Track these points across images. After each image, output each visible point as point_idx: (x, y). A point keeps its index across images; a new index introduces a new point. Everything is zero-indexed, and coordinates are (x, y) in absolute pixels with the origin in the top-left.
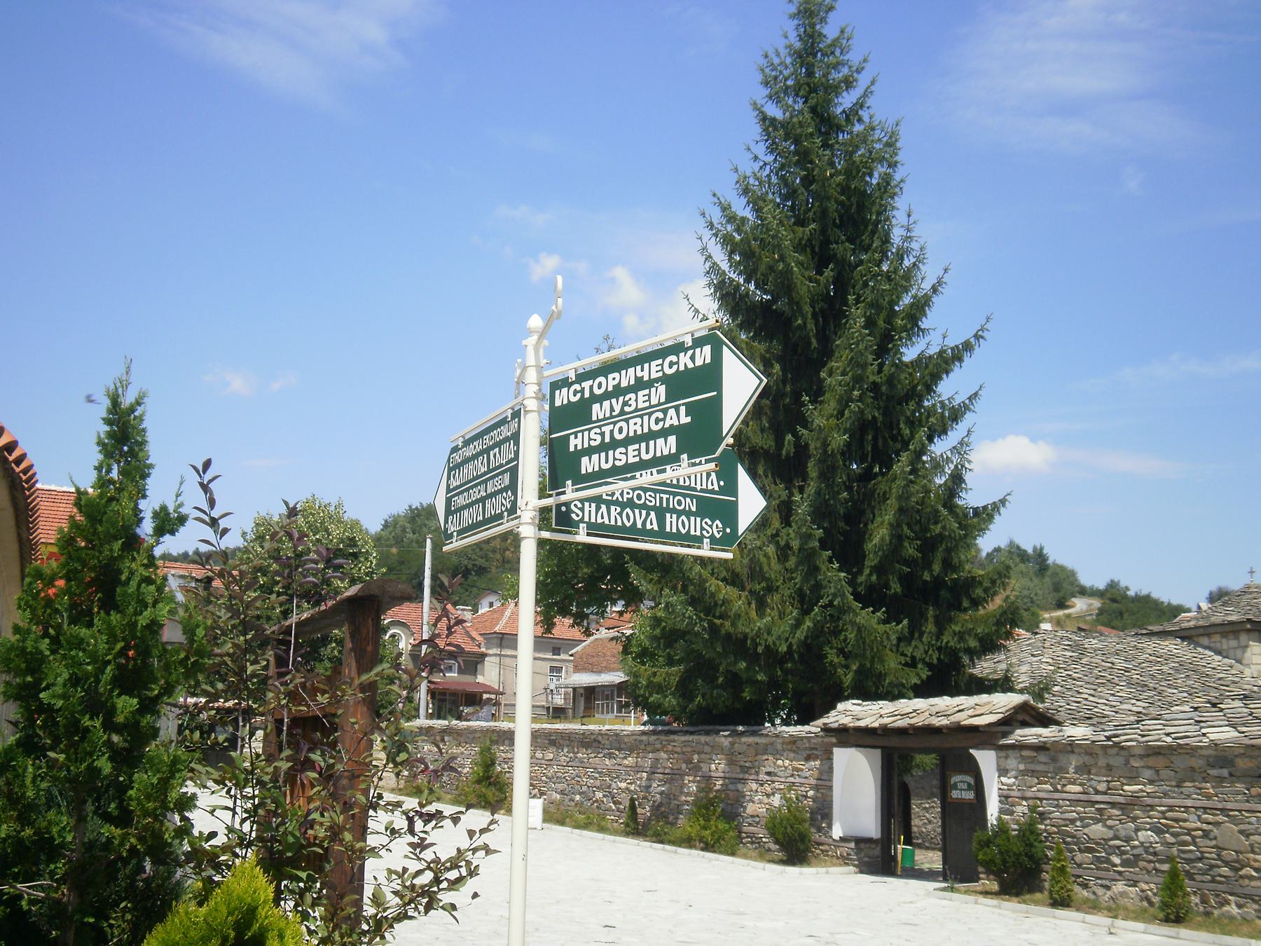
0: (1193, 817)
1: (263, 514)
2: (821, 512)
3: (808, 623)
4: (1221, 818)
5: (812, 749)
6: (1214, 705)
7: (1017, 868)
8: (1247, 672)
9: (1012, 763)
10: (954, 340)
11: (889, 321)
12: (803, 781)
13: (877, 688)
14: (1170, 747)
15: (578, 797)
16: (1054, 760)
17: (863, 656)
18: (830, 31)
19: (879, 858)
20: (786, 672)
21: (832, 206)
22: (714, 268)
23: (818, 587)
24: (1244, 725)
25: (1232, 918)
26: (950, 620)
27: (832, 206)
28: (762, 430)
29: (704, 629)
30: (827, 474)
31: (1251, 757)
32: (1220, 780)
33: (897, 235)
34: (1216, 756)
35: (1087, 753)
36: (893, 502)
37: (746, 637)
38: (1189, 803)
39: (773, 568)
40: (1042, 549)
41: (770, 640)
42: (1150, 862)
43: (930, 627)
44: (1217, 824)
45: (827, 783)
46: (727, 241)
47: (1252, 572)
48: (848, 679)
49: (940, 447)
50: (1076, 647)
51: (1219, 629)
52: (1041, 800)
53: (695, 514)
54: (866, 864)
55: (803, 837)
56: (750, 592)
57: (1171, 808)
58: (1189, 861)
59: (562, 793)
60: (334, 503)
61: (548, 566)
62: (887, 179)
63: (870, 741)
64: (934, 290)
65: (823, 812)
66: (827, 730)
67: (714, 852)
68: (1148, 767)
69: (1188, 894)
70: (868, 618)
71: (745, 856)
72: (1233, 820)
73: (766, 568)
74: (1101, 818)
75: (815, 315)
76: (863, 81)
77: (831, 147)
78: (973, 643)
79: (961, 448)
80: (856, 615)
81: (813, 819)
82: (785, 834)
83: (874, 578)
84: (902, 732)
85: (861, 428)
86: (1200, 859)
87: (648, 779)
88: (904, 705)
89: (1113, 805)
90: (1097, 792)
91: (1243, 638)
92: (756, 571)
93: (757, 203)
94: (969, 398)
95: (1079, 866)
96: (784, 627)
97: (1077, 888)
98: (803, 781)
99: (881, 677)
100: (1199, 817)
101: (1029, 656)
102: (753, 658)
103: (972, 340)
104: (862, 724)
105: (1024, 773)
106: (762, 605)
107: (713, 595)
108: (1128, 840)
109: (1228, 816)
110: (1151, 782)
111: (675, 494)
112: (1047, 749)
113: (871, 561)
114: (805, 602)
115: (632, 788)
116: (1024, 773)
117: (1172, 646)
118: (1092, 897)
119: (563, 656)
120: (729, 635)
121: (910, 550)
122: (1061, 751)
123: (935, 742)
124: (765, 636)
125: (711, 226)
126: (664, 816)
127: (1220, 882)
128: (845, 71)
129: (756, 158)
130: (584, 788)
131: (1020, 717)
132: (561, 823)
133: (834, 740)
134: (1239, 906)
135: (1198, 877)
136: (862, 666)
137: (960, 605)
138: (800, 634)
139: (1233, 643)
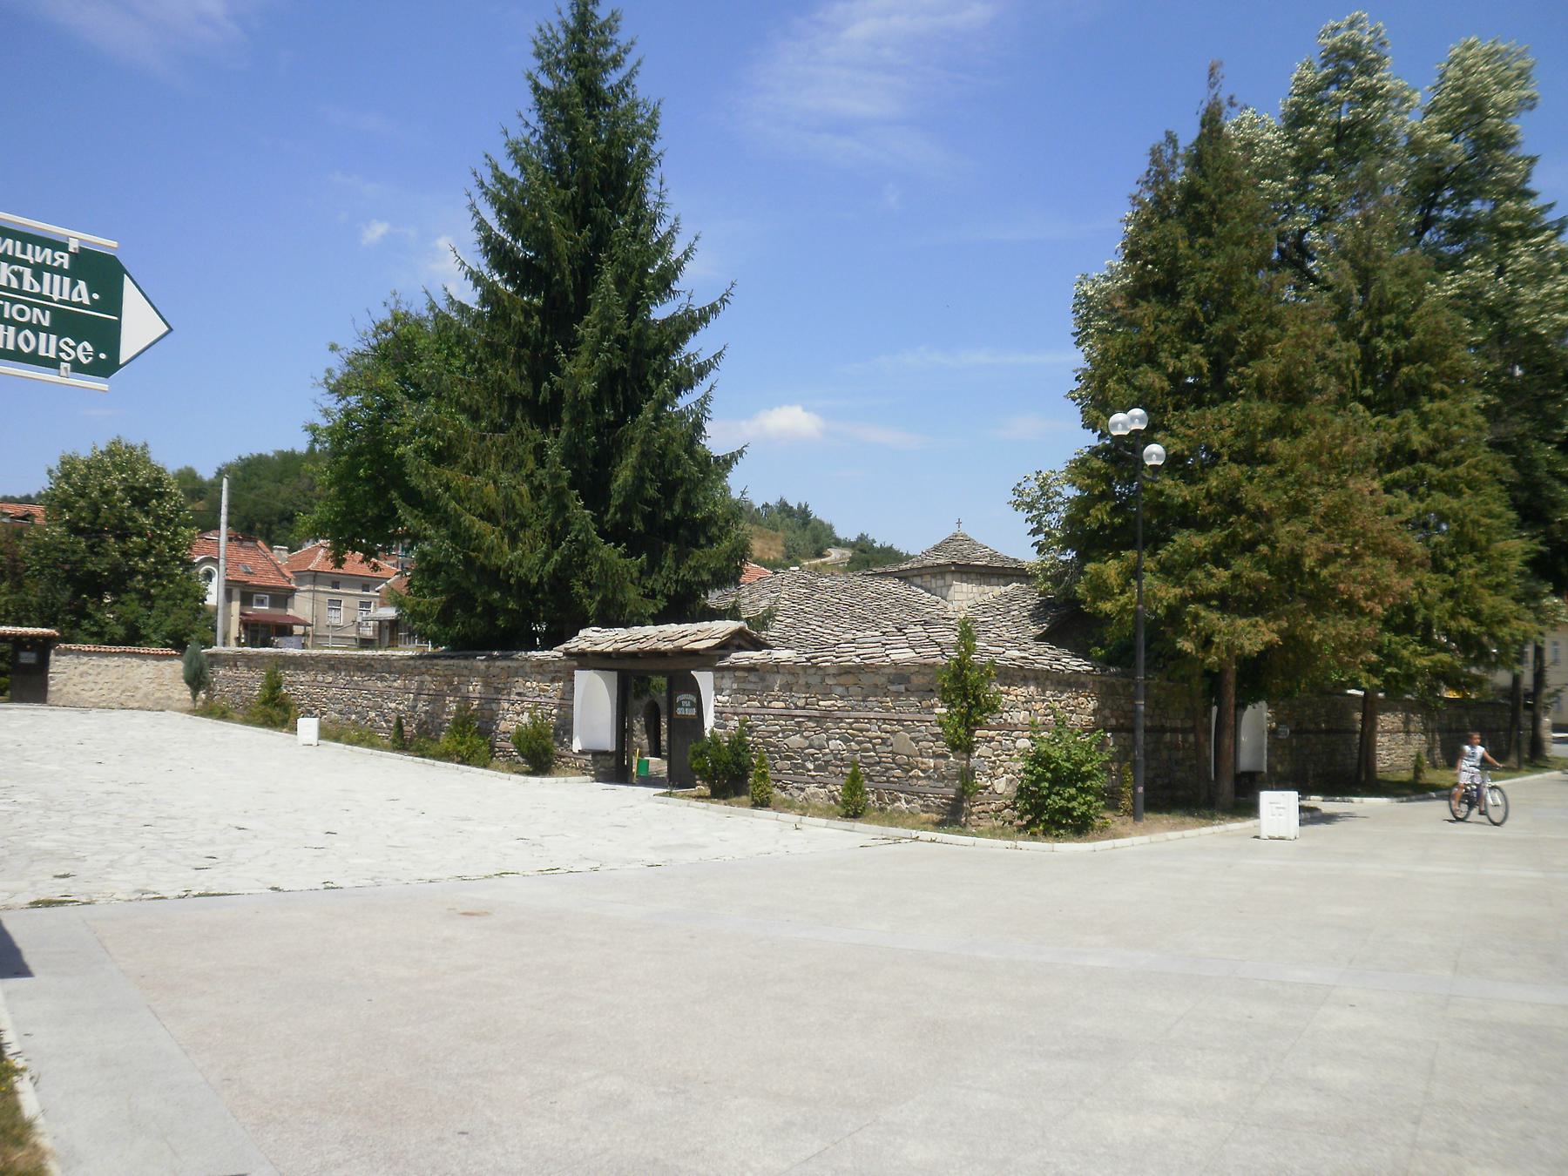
1: (69, 452)
2: (572, 455)
3: (556, 557)
4: (897, 728)
7: (729, 775)
8: (950, 607)
9: (727, 683)
10: (699, 303)
11: (640, 281)
14: (858, 667)
16: (763, 679)
17: (605, 587)
18: (602, 13)
19: (614, 768)
20: (538, 602)
21: (594, 172)
22: (482, 225)
23: (567, 523)
25: (902, 812)
27: (594, 172)
28: (522, 378)
30: (576, 421)
32: (899, 694)
33: (651, 198)
36: (636, 449)
37: (499, 568)
38: (872, 715)
39: (525, 506)
43: (669, 562)
44: (893, 733)
46: (494, 199)
48: (592, 608)
49: (685, 401)
50: (811, 586)
53: (47, 330)
55: (547, 751)
56: (505, 528)
57: (857, 720)
58: (869, 765)
59: (340, 712)
60: (140, 444)
62: (645, 151)
63: (607, 664)
64: (686, 254)
65: (565, 728)
66: (567, 653)
70: (608, 552)
71: (496, 769)
72: (907, 729)
73: (518, 505)
75: (573, 273)
76: (629, 61)
77: (595, 117)
78: (706, 577)
79: (704, 402)
81: (556, 735)
82: (530, 748)
84: (633, 655)
85: (610, 380)
88: (637, 632)
89: (810, 718)
90: (797, 707)
91: (949, 578)
92: (511, 511)
93: (523, 162)
95: (780, 771)
96: (534, 559)
97: (776, 791)
99: (623, 606)
101: (759, 589)
102: (505, 587)
104: (598, 648)
105: (737, 691)
106: (514, 540)
107: (467, 529)
108: (821, 748)
110: (842, 698)
111: (13, 302)
113: (616, 501)
114: (555, 536)
116: (737, 691)
117: (890, 585)
119: (371, 593)
120: (483, 568)
121: (651, 491)
123: (661, 664)
125: (482, 185)
126: (427, 733)
128: (613, 50)
129: (527, 125)
131: (736, 642)
132: (337, 739)
134: (908, 802)
136: (605, 596)
138: (549, 567)
139: (940, 583)
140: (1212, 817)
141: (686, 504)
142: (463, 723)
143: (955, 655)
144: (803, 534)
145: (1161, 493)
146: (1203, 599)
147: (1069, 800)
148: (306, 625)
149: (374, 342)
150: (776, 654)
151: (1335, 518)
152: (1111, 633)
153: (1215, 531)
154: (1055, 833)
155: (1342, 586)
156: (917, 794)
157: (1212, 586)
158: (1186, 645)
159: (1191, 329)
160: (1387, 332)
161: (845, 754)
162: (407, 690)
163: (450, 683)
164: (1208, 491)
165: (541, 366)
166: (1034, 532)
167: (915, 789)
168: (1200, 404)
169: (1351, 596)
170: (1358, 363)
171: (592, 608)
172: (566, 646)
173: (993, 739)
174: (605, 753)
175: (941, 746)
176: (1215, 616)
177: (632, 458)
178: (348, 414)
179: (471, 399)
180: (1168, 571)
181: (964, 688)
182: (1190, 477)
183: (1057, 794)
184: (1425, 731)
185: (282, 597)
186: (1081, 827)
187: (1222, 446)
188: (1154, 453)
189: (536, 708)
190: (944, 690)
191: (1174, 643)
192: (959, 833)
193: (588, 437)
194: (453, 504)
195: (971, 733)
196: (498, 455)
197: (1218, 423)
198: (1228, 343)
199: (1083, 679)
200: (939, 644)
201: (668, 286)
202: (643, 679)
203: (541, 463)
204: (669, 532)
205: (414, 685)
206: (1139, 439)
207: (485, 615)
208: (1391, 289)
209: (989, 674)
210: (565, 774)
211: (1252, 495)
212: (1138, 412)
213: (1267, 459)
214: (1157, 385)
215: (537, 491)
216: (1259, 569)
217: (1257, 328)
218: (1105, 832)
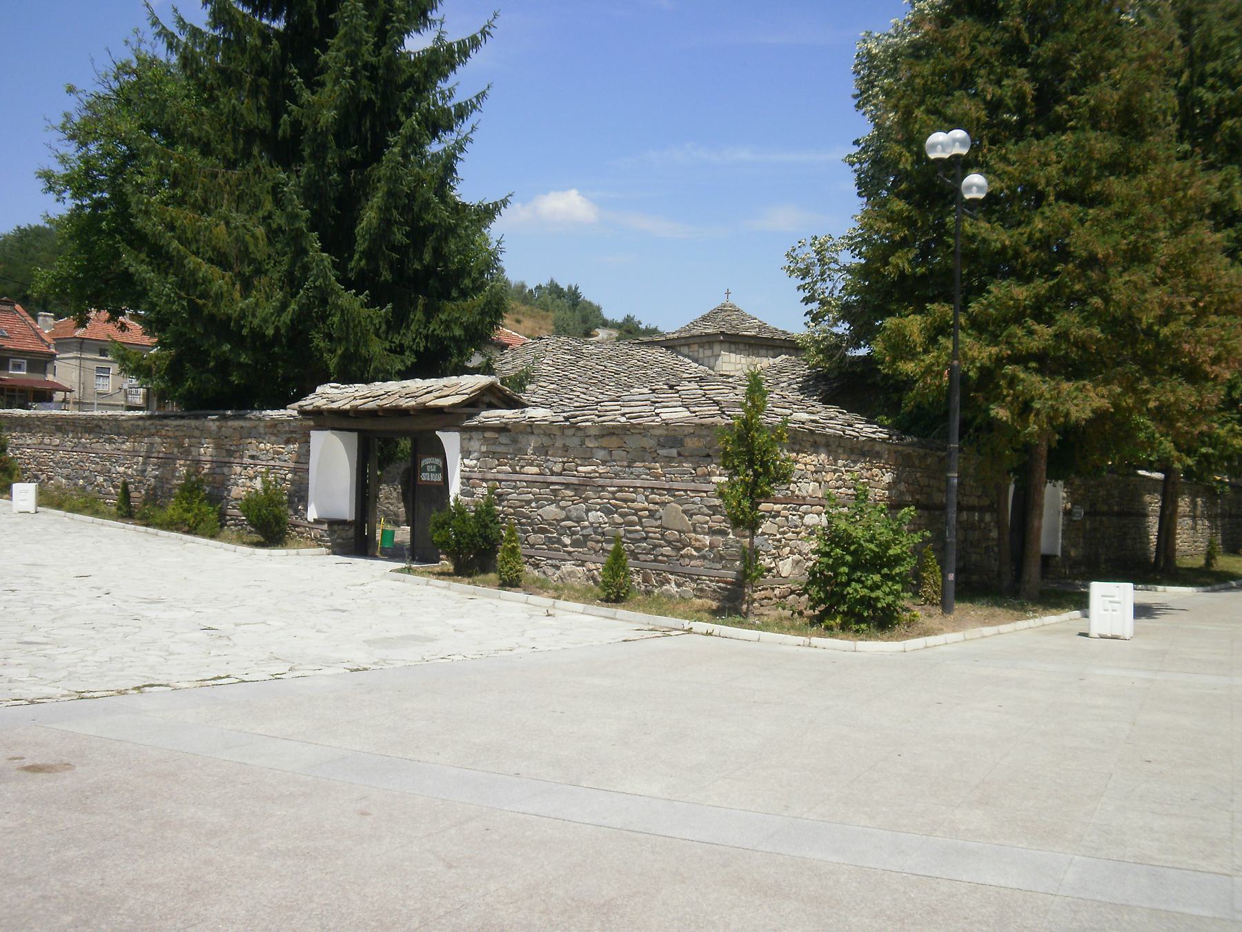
0: (641, 498)
2: (312, 193)
3: (294, 306)
4: (667, 498)
5: (292, 432)
6: (671, 387)
7: (473, 549)
9: (476, 445)
12: (282, 464)
13: (363, 374)
15: (81, 482)
16: (515, 441)
19: (354, 539)
23: (306, 269)
24: (696, 405)
25: (671, 597)
26: (438, 310)
28: (259, 110)
29: (183, 308)
31: (700, 436)
32: (670, 459)
34: (667, 436)
35: (545, 434)
36: (383, 187)
37: (229, 318)
38: (638, 483)
39: (261, 249)
40: (576, 288)
41: (256, 322)
42: (598, 542)
43: (419, 315)
44: (663, 504)
45: (305, 466)
47: (728, 293)
48: (333, 362)
51: (697, 340)
52: (500, 481)
54: (339, 545)
55: (279, 520)
57: (621, 489)
58: (634, 541)
59: (67, 477)
61: (77, 260)
63: (345, 424)
65: (300, 495)
66: (302, 412)
67: (196, 534)
68: (604, 448)
69: (632, 573)
70: (349, 300)
73: (252, 248)
74: (555, 499)
78: (458, 332)
80: (339, 297)
81: (290, 502)
82: (258, 517)
83: (363, 263)
84: (372, 414)
85: (353, 110)
86: (645, 539)
87: (144, 463)
88: (378, 387)
89: (567, 486)
90: (553, 473)
91: (717, 348)
92: (245, 255)
94: (477, 97)
95: (532, 546)
96: (269, 308)
97: (527, 568)
98: (282, 464)
99: (367, 361)
100: (647, 497)
102: (239, 341)
103: (479, 36)
104: (335, 406)
105: (485, 455)
106: (247, 288)
107: (193, 273)
108: (578, 520)
109: (674, 496)
110: (604, 463)
112: (509, 431)
113: (361, 246)
114: (292, 283)
115: (130, 471)
116: (485, 455)
118: (542, 576)
120: (212, 317)
121: (399, 236)
122: (521, 433)
123: (404, 424)
124: (250, 318)
127: (661, 562)
130: (87, 473)
131: (486, 399)
132: (59, 506)
133: (312, 423)
134: (679, 585)
135: (642, 557)
136: (347, 349)
137: (450, 293)
138: (286, 317)
139: (708, 353)
140: (1023, 609)
141: (438, 254)
142: (191, 489)
143: (739, 412)
144: (572, 314)
145: (972, 239)
146: (1017, 359)
147: (872, 589)
148: (66, 390)
149: (116, 86)
150: (530, 412)
151: (1180, 267)
152: (909, 401)
153: (1038, 282)
154: (855, 627)
155: (1186, 347)
156: (690, 576)
157: (1035, 344)
158: (1000, 413)
159: (1015, 51)
160: (1210, 81)
161: (607, 527)
162: (135, 453)
163: (180, 446)
164: (1030, 236)
165: (279, 99)
166: (807, 300)
167: (687, 570)
168: (1020, 137)
169: (1193, 360)
170: (1174, 116)
171: (333, 362)
172: (301, 403)
173: (778, 514)
174: (343, 522)
175: (718, 522)
176: (1036, 378)
177: (377, 199)
178: (86, 161)
179: (200, 129)
180: (979, 326)
181: (750, 452)
182: (1009, 222)
183: (859, 581)
184: (1209, 518)
185: (41, 362)
186: (883, 621)
187: (1048, 184)
188: (975, 184)
189: (267, 472)
190: (726, 455)
191: (987, 410)
192: (741, 625)
193: (329, 174)
194: (175, 243)
195: (754, 506)
196: (231, 193)
197: (1045, 159)
198: (1058, 64)
199: (877, 448)
200: (717, 403)
201: (424, 14)
202: (389, 441)
203: (278, 202)
204: (420, 282)
205: (143, 448)
206: (959, 166)
207: (224, 372)
208: (1218, 33)
209: (781, 437)
210: (299, 546)
211: (1084, 239)
212: (959, 134)
213: (1101, 200)
214: (974, 114)
215: (273, 234)
216: (1091, 325)
217: (1095, 48)
218: (913, 628)
